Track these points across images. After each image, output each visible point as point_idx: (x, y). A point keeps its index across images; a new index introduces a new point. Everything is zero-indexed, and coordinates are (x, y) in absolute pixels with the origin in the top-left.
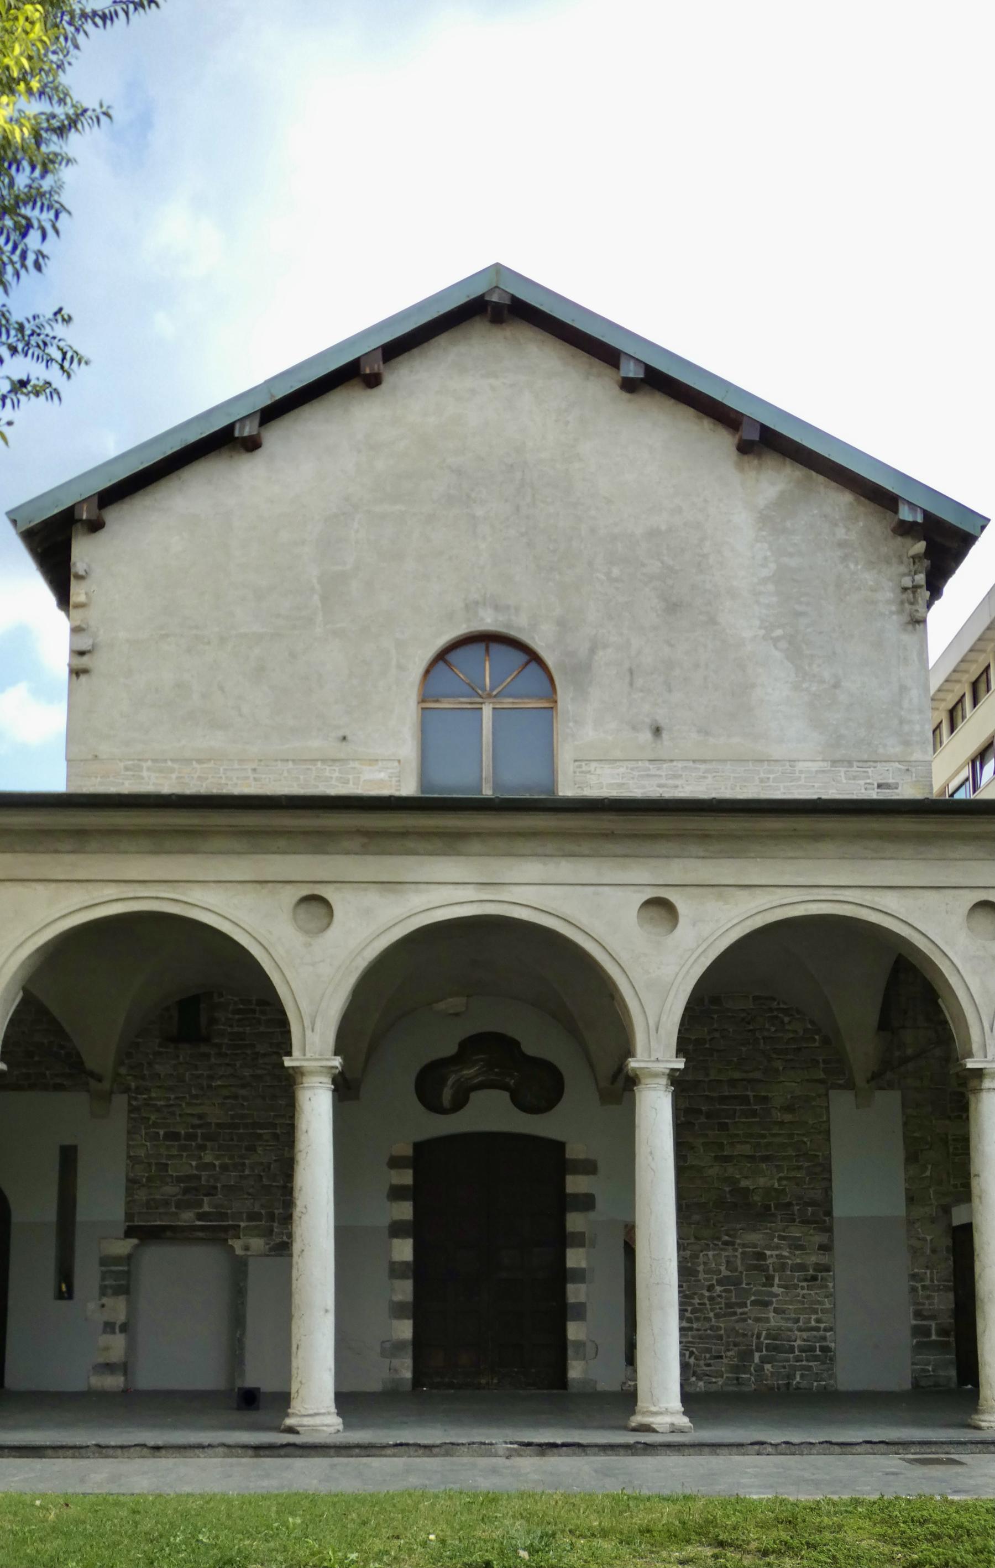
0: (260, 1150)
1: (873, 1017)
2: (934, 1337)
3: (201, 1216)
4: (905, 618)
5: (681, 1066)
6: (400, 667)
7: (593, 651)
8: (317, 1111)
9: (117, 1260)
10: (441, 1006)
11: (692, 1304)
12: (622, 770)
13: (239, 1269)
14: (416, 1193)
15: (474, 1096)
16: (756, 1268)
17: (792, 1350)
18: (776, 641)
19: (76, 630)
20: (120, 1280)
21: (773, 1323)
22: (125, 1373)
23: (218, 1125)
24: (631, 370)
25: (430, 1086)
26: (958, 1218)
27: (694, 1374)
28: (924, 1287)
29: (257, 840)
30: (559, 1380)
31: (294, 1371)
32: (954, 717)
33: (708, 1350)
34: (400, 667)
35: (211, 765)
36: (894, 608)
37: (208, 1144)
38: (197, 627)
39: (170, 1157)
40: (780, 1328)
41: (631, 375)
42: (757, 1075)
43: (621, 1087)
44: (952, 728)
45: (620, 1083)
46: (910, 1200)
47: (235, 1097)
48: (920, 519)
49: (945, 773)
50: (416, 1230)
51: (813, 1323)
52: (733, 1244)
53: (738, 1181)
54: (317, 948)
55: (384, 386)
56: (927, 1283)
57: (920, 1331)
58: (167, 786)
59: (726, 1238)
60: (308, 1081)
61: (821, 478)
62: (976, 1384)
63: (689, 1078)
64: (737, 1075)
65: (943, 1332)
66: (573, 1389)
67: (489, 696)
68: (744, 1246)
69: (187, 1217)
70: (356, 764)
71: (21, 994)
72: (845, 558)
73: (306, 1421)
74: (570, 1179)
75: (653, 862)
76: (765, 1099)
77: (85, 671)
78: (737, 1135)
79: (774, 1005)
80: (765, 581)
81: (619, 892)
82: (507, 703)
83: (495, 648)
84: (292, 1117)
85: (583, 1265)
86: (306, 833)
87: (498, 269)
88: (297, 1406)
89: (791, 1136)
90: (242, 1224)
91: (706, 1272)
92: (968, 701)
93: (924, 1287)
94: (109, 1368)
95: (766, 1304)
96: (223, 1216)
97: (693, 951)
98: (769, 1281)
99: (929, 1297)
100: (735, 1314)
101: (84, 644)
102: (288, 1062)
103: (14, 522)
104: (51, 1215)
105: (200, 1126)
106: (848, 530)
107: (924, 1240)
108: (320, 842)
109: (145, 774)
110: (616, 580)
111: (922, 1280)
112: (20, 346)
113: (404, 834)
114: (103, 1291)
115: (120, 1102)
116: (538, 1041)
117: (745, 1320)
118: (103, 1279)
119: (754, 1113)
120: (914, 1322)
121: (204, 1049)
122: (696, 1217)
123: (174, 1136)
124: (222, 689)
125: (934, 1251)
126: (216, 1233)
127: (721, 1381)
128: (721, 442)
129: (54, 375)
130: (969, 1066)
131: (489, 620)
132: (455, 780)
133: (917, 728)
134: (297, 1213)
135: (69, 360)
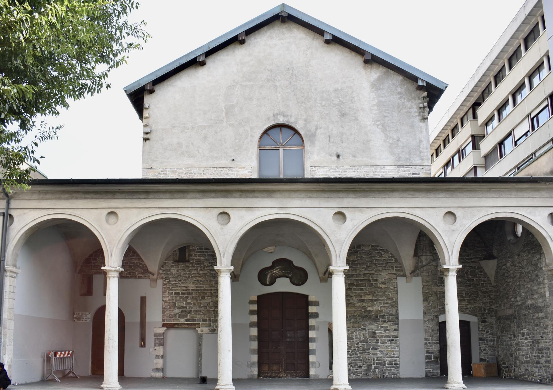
0: (206, 298)
1: (412, 252)
3: (187, 320)
4: (420, 118)
5: (348, 268)
6: (252, 136)
7: (316, 129)
8: (225, 284)
9: (160, 335)
10: (265, 250)
12: (326, 169)
13: (200, 337)
14: (259, 313)
15: (277, 280)
16: (373, 337)
17: (385, 364)
18: (378, 125)
19: (145, 126)
20: (161, 341)
22: (163, 372)
23: (192, 290)
24: (328, 37)
25: (263, 277)
26: (441, 319)
27: (352, 372)
28: (429, 343)
29: (205, 193)
30: (307, 375)
31: (219, 371)
32: (437, 152)
33: (357, 365)
34: (252, 136)
35: (189, 169)
36: (417, 114)
37: (189, 296)
38: (184, 124)
39: (177, 300)
40: (381, 357)
41: (328, 38)
42: (373, 272)
43: (328, 275)
44: (437, 156)
45: (327, 275)
46: (425, 313)
47: (198, 280)
48: (425, 85)
49: (435, 170)
50: (259, 325)
52: (365, 329)
53: (367, 308)
55: (246, 44)
57: (427, 357)
58: (175, 177)
59: (363, 327)
60: (222, 274)
61: (392, 71)
62: (447, 375)
63: (350, 273)
64: (366, 272)
65: (436, 358)
66: (311, 378)
67: (282, 145)
68: (369, 329)
69: (182, 320)
70: (237, 169)
71: (128, 246)
72: (400, 98)
73: (223, 387)
74: (310, 307)
75: (338, 200)
76: (376, 280)
77: (148, 139)
78: (366, 292)
79: (379, 248)
80: (374, 105)
81: (326, 210)
82: (288, 147)
83: (284, 129)
84: (217, 287)
85: (315, 336)
86: (221, 191)
87: (283, 5)
88: (220, 382)
89: (384, 292)
90: (201, 323)
92: (442, 146)
93: (429, 343)
94: (157, 370)
95: (376, 349)
96: (194, 320)
97: (352, 230)
99: (431, 346)
101: (148, 130)
102: (216, 268)
103: (126, 91)
104: (138, 320)
105: (186, 290)
106: (401, 88)
107: (429, 327)
108: (226, 194)
109: (167, 173)
110: (324, 106)
112: (130, 33)
113: (254, 191)
114: (155, 346)
115: (160, 282)
116: (299, 261)
117: (369, 354)
118: (155, 341)
119: (372, 285)
121: (187, 264)
122: (353, 320)
124: (192, 144)
125: (432, 331)
126: (192, 325)
127: (361, 375)
128: (358, 60)
129: (141, 41)
130: (445, 267)
131: (281, 120)
132: (270, 174)
133: (426, 154)
134: (219, 318)
135: (145, 37)
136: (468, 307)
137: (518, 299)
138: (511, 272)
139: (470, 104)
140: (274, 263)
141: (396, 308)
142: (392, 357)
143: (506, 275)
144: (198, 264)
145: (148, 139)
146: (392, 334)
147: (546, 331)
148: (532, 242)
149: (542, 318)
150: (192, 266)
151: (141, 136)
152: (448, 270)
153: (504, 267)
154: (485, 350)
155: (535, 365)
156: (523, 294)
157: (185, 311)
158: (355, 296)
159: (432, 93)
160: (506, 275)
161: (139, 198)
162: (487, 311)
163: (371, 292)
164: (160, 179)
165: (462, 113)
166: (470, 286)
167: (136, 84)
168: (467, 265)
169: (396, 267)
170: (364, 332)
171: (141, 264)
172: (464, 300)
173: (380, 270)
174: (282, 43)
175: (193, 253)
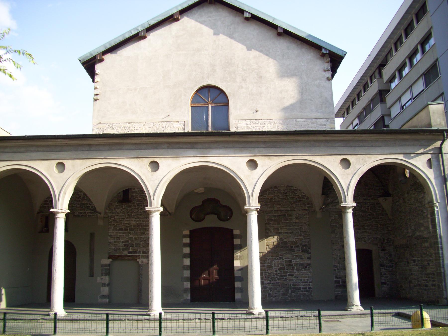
1: (320, 192)
2: (341, 284)
3: (129, 253)
9: (106, 265)
11: (271, 276)
19: (96, 88)
21: (294, 281)
23: (134, 226)
28: (338, 269)
33: (276, 289)
37: (131, 232)
39: (120, 236)
42: (288, 209)
47: (139, 218)
48: (327, 53)
51: (306, 281)
54: (156, 177)
56: (339, 268)
59: (280, 256)
64: (282, 209)
68: (285, 258)
69: (125, 253)
76: (291, 216)
77: (98, 99)
79: (293, 188)
86: (152, 143)
90: (141, 255)
91: (275, 266)
93: (338, 269)
94: (104, 297)
95: (292, 275)
98: (293, 269)
99: (339, 272)
100: (283, 278)
103: (80, 60)
105: (129, 227)
110: (245, 70)
111: (337, 267)
117: (286, 280)
118: (102, 271)
119: (287, 220)
120: (335, 279)
121: (130, 204)
123: (121, 230)
125: (340, 259)
130: (342, 205)
136: (370, 237)
137: (410, 231)
138: (403, 207)
139: (376, 65)
140: (204, 202)
141: (309, 240)
142: (306, 282)
143: (400, 210)
144: (139, 204)
145: (98, 99)
146: (306, 262)
147: (431, 259)
148: (417, 183)
149: (428, 247)
150: (134, 206)
151: (92, 97)
152: (345, 208)
153: (397, 203)
154: (385, 274)
155: (425, 288)
156: (413, 227)
157: (128, 245)
158: (273, 229)
159: (334, 59)
160: (400, 210)
161: (83, 151)
162: (386, 241)
163: (287, 226)
164: (100, 135)
165: (371, 73)
166: (371, 219)
167: (89, 55)
168: (368, 201)
169: (307, 204)
170: (281, 260)
171: (91, 205)
172: (366, 232)
173: (294, 207)
174: (210, 20)
175: (134, 194)
